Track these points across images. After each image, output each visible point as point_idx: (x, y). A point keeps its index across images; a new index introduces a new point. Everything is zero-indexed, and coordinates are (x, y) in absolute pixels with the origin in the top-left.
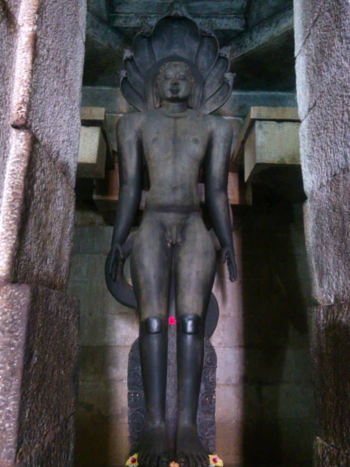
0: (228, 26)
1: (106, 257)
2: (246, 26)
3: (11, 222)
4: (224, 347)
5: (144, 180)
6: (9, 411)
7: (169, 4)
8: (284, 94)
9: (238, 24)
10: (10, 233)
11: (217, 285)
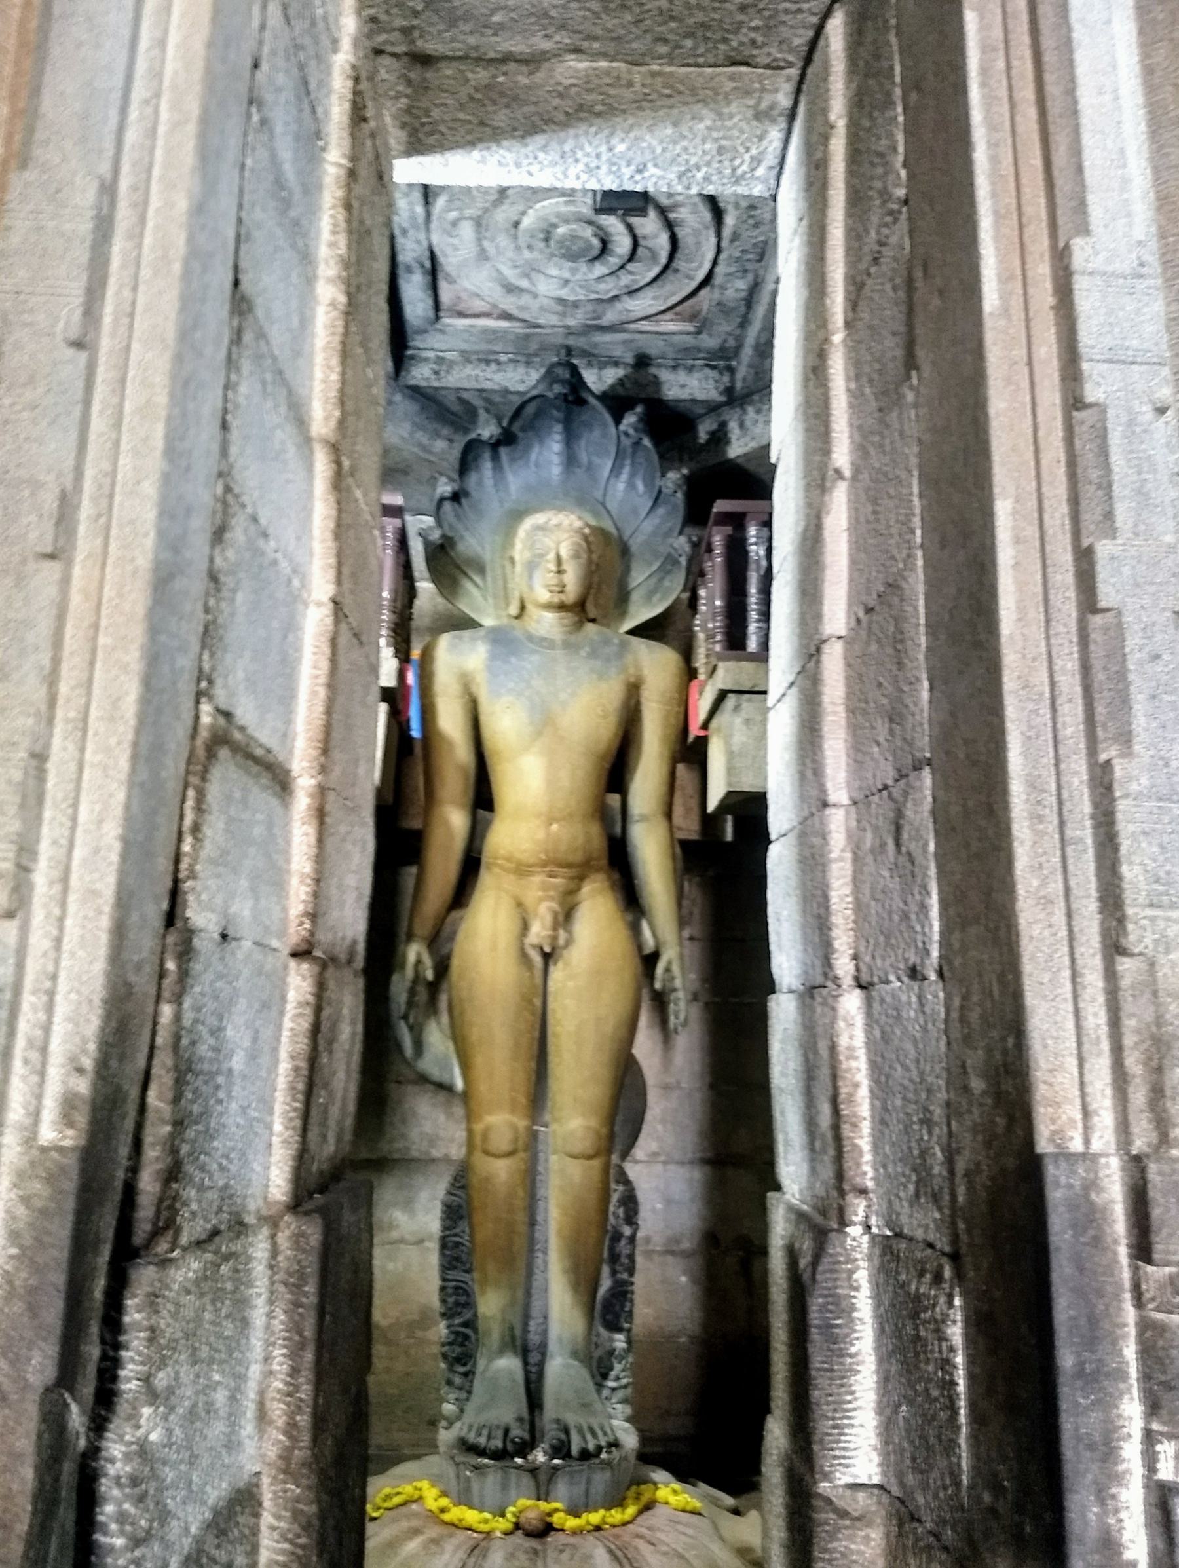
3: (292, 1115)
4: (665, 1163)
5: (482, 798)
6: (301, 1400)
9: (711, 385)
10: (291, 1132)
11: (650, 1026)
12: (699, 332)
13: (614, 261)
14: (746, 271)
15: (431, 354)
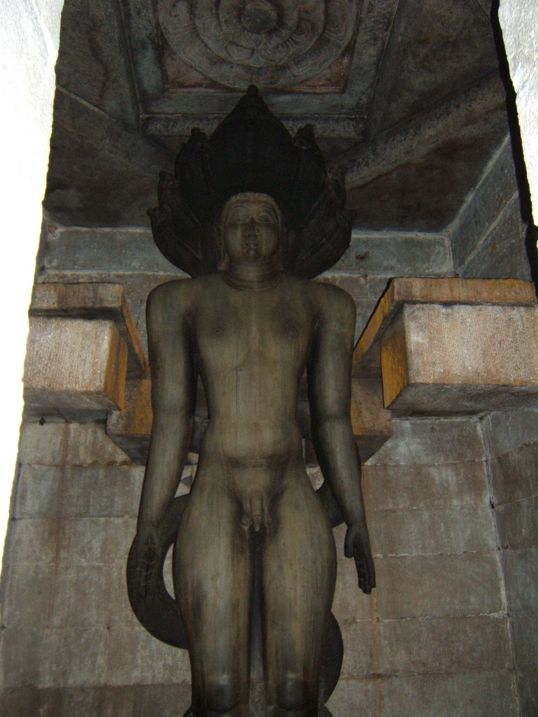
0: (336, 133)
1: (135, 521)
2: (365, 134)
7: (239, 99)
8: (430, 236)
12: (343, 91)
13: (284, 32)
14: (376, 39)
15: (163, 116)
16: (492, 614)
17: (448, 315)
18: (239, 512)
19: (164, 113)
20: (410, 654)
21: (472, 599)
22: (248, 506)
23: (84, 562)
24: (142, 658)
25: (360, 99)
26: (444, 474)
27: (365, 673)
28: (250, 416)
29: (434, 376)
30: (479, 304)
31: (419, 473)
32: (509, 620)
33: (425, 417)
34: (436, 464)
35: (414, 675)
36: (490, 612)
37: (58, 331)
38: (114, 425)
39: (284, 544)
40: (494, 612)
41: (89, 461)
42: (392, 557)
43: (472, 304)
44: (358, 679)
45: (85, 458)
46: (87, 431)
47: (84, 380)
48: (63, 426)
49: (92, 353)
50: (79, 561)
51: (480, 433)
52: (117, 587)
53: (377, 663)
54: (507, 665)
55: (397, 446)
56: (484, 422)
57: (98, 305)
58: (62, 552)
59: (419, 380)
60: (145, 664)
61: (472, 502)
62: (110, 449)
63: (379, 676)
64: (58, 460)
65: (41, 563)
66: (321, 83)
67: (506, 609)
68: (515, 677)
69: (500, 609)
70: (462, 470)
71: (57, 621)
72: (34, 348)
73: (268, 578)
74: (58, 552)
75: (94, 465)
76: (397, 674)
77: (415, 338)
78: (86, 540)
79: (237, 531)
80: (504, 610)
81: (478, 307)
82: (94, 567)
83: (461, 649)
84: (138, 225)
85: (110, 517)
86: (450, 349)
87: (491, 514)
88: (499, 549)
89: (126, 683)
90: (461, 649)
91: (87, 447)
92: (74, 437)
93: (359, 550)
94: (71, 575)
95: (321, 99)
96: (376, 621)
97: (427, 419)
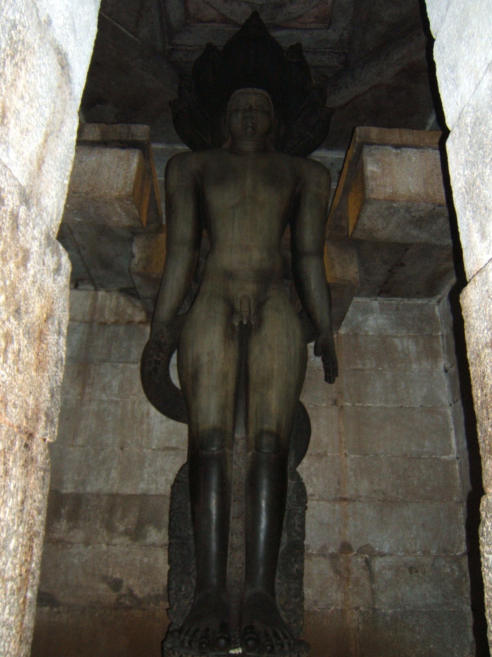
12: (328, 28)
16: (443, 457)
17: (397, 154)
18: (232, 311)
19: (185, 45)
20: (372, 483)
21: (427, 443)
22: (239, 307)
23: (104, 397)
24: (148, 473)
25: (342, 35)
26: (405, 343)
27: (333, 496)
28: (243, 244)
29: (385, 194)
30: (422, 148)
31: (384, 342)
32: (457, 462)
33: (391, 298)
34: (399, 335)
35: (375, 501)
36: (442, 455)
37: (100, 155)
38: (136, 265)
39: (265, 334)
40: (445, 455)
41: (112, 320)
42: (359, 406)
43: (417, 147)
44: (328, 501)
45: (109, 317)
46: (111, 296)
47: (117, 188)
48: (93, 293)
49: (125, 170)
50: (101, 396)
51: (437, 313)
52: (130, 417)
53: (343, 489)
54: (455, 499)
55: (367, 320)
56: (441, 304)
57: (130, 139)
58: (87, 388)
59: (373, 196)
60: (151, 479)
61: (429, 367)
62: (129, 311)
63: (345, 500)
64: (87, 318)
65: (69, 396)
66: (310, 20)
67: (456, 453)
68: (462, 508)
69: (450, 453)
70: (421, 341)
71: (80, 441)
72: (81, 166)
73: (252, 358)
74: (83, 388)
75: (116, 323)
76: (361, 499)
77: (371, 168)
78: (107, 380)
79: (229, 325)
80: (454, 454)
81: (421, 150)
82: (112, 401)
83: (416, 482)
84: (161, 142)
85: (127, 363)
86: (398, 177)
87: (444, 377)
88: (451, 405)
89: (133, 493)
90: (416, 482)
91: (111, 309)
92: (101, 301)
93: (327, 352)
94: (94, 406)
95: (310, 34)
96: (344, 455)
97: (393, 300)
